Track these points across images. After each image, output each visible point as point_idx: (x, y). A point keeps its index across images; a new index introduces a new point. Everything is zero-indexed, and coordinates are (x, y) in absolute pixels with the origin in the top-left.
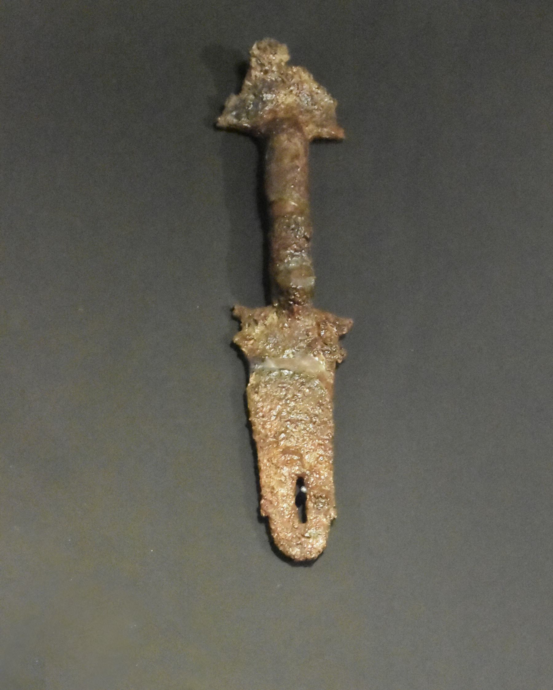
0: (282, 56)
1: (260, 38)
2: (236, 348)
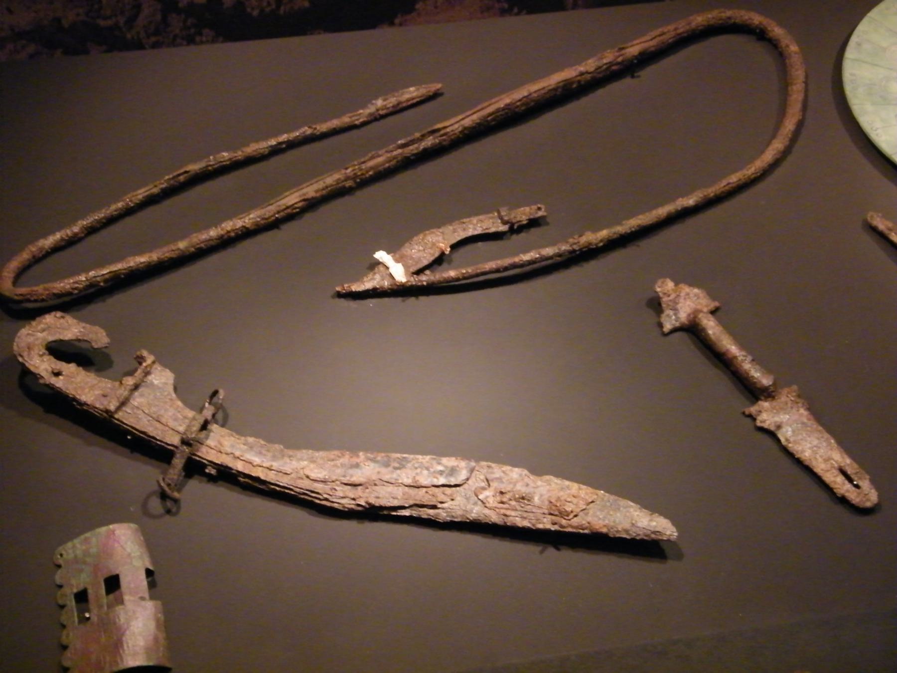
0: (670, 285)
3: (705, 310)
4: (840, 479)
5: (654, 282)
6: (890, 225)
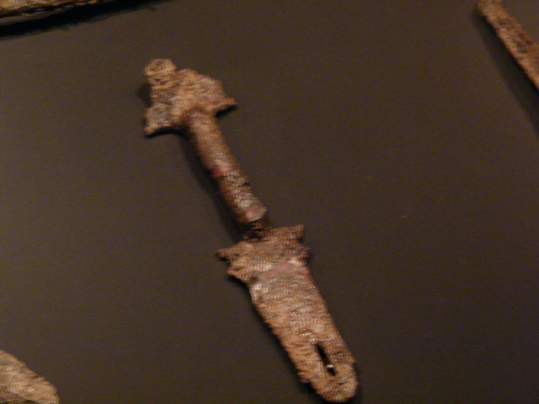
0: (168, 68)
1: (147, 63)
2: (233, 279)
3: (210, 108)
4: (314, 358)
5: (147, 63)
6: (504, 16)
